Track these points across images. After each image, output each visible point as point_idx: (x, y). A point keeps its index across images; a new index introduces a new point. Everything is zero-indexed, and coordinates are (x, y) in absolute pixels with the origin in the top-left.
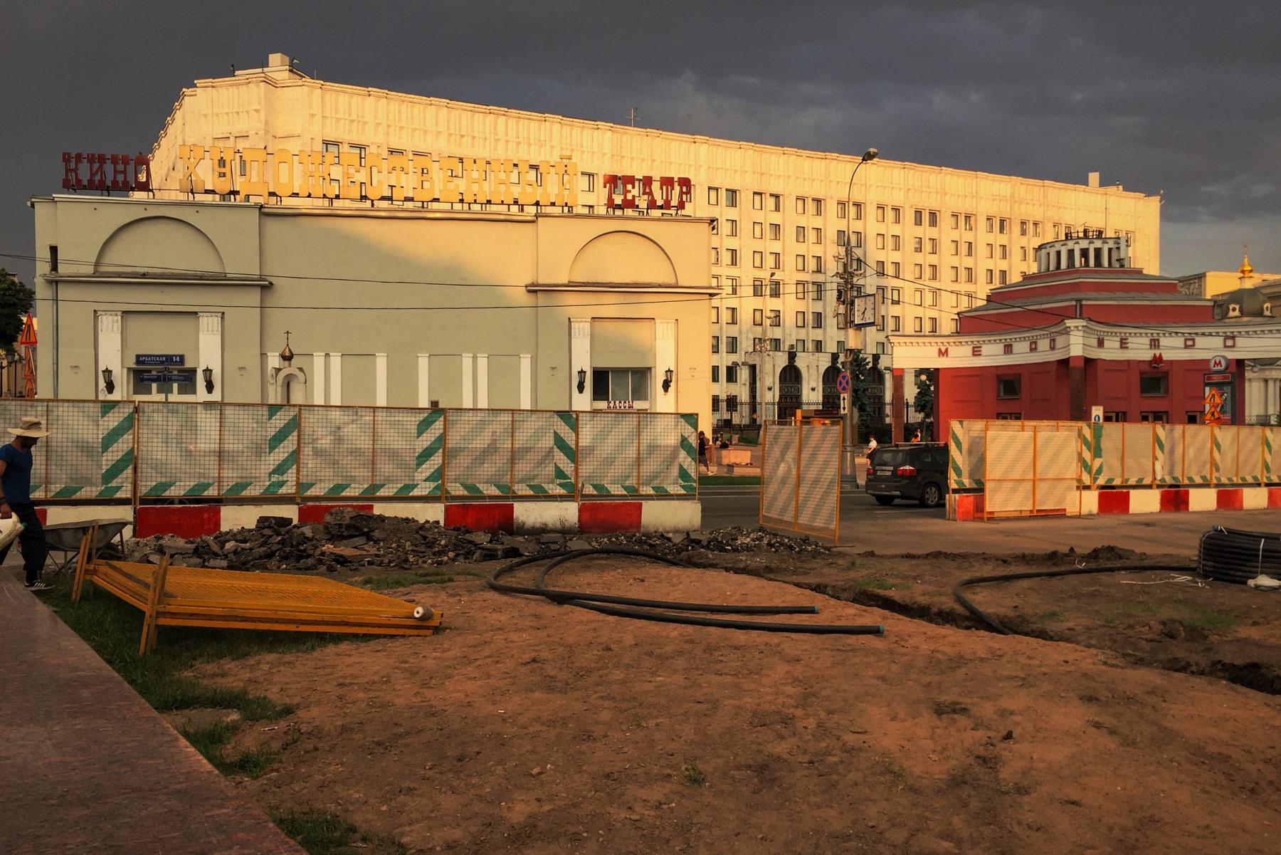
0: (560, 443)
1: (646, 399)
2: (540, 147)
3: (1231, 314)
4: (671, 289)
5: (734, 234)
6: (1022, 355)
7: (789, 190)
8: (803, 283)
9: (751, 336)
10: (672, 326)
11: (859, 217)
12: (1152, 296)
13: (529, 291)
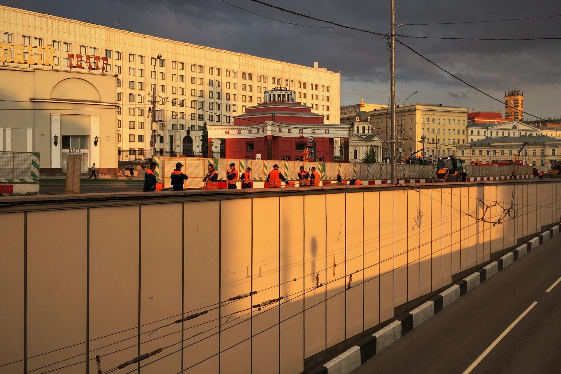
0: (33, 163)
1: (87, 149)
2: (70, 34)
3: (357, 120)
4: (98, 103)
5: (163, 79)
6: (255, 135)
7: (189, 61)
8: (194, 101)
9: (171, 123)
10: (98, 118)
11: (219, 74)
12: (302, 113)
13: (31, 102)
